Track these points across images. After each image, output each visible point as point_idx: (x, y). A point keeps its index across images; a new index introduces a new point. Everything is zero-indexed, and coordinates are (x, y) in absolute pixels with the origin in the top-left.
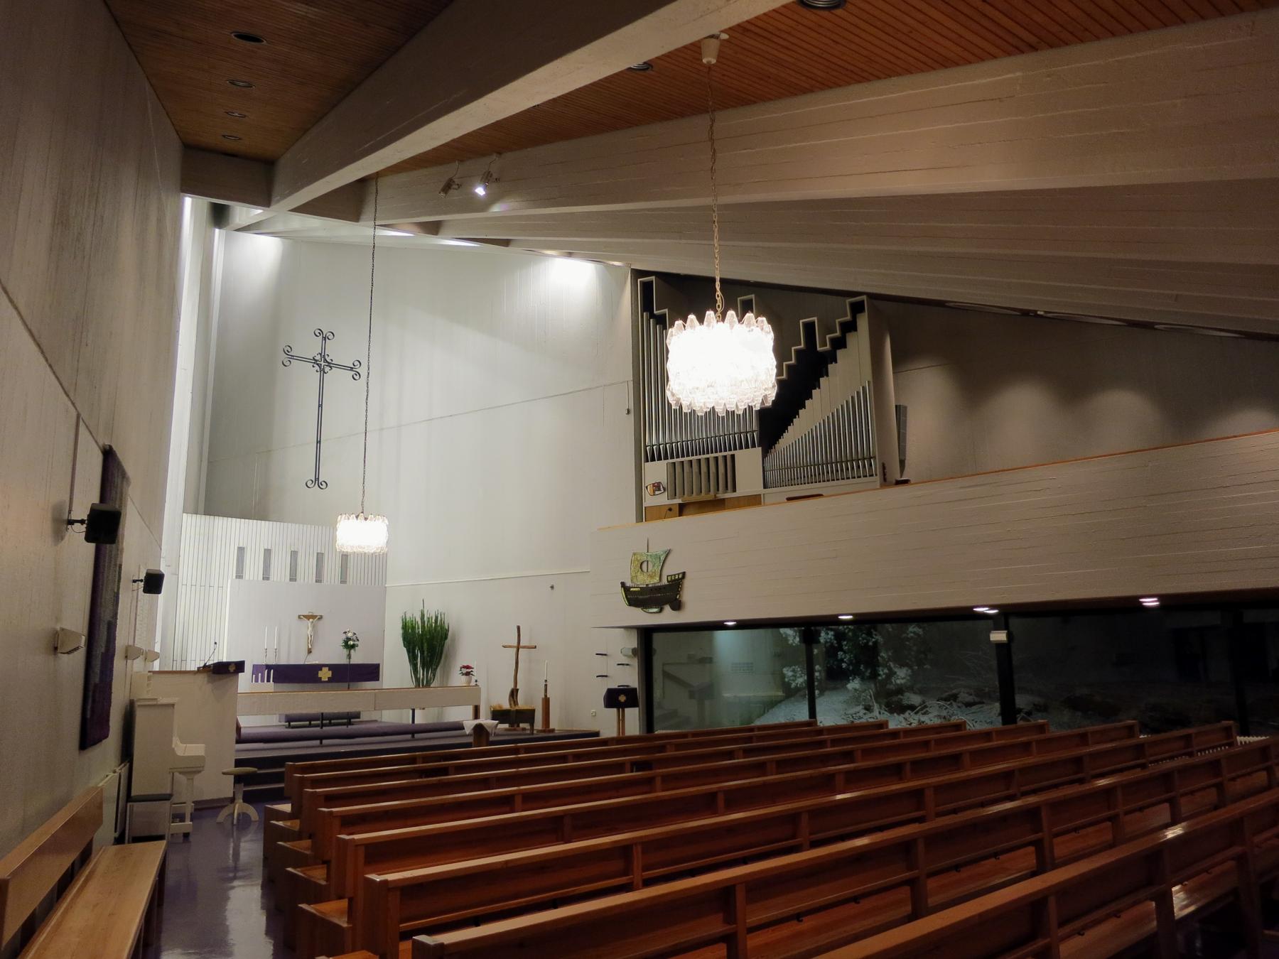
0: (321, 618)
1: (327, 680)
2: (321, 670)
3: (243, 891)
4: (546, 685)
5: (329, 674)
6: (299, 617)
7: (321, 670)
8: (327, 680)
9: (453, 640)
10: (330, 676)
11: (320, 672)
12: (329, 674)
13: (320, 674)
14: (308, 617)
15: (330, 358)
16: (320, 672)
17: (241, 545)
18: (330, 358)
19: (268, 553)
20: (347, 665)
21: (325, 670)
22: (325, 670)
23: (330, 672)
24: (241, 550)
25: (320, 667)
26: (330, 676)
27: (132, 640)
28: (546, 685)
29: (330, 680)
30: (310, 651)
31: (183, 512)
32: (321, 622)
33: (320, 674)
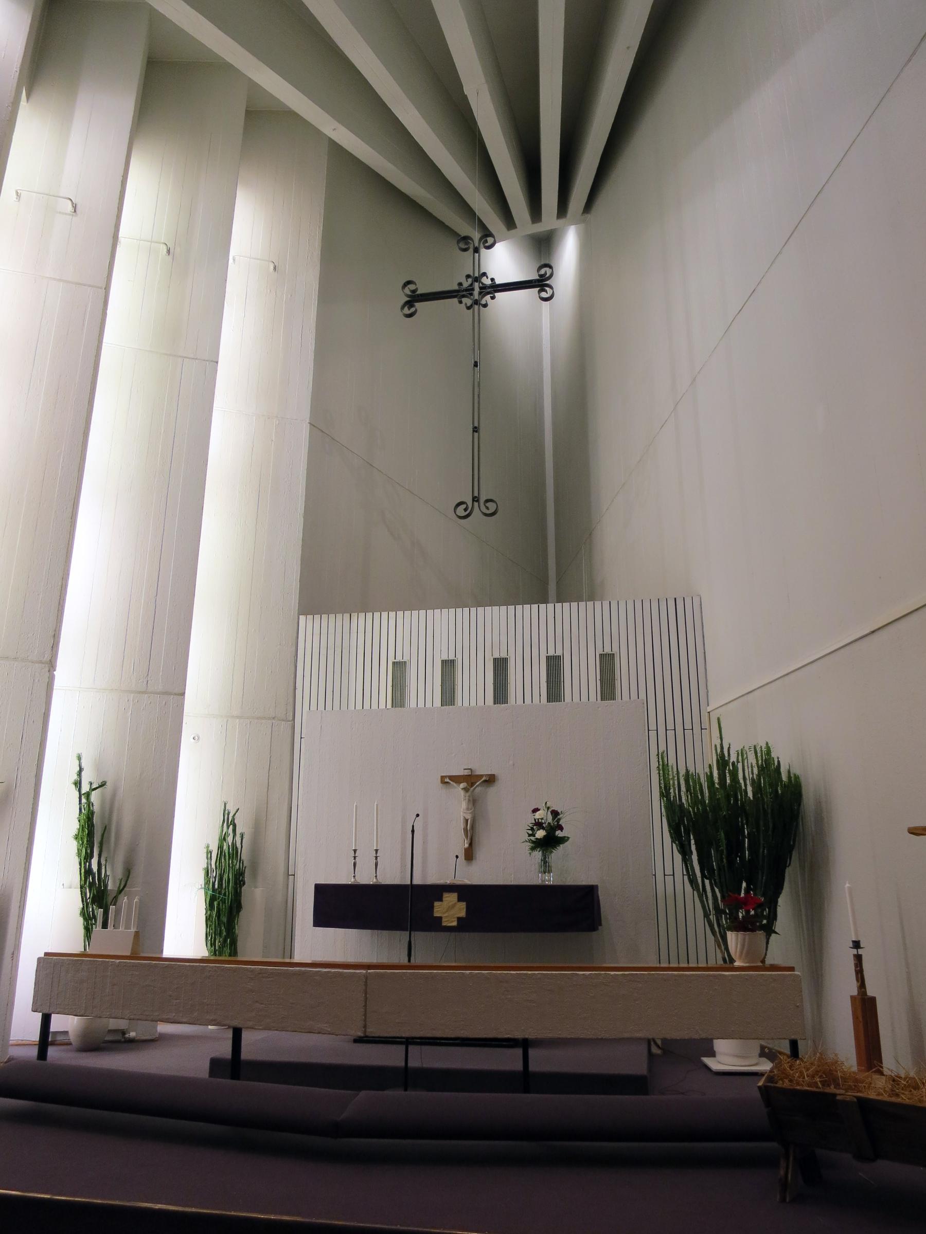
0: (491, 780)
1: (455, 924)
2: (440, 899)
3: (921, 1101)
4: (858, 959)
5: (461, 910)
6: (443, 777)
7: (440, 899)
8: (455, 924)
9: (821, 819)
10: (463, 914)
11: (436, 904)
12: (461, 910)
13: (439, 909)
14: (456, 779)
15: (463, 280)
16: (436, 904)
17: (399, 659)
18: (463, 280)
19: (448, 666)
20: (405, 886)
21: (450, 898)
22: (450, 898)
23: (463, 905)
24: (399, 667)
25: (436, 891)
26: (463, 914)
27: (684, 878)
28: (858, 959)
29: (463, 925)
30: (469, 855)
31: (299, 614)
32: (492, 790)
33: (439, 909)
